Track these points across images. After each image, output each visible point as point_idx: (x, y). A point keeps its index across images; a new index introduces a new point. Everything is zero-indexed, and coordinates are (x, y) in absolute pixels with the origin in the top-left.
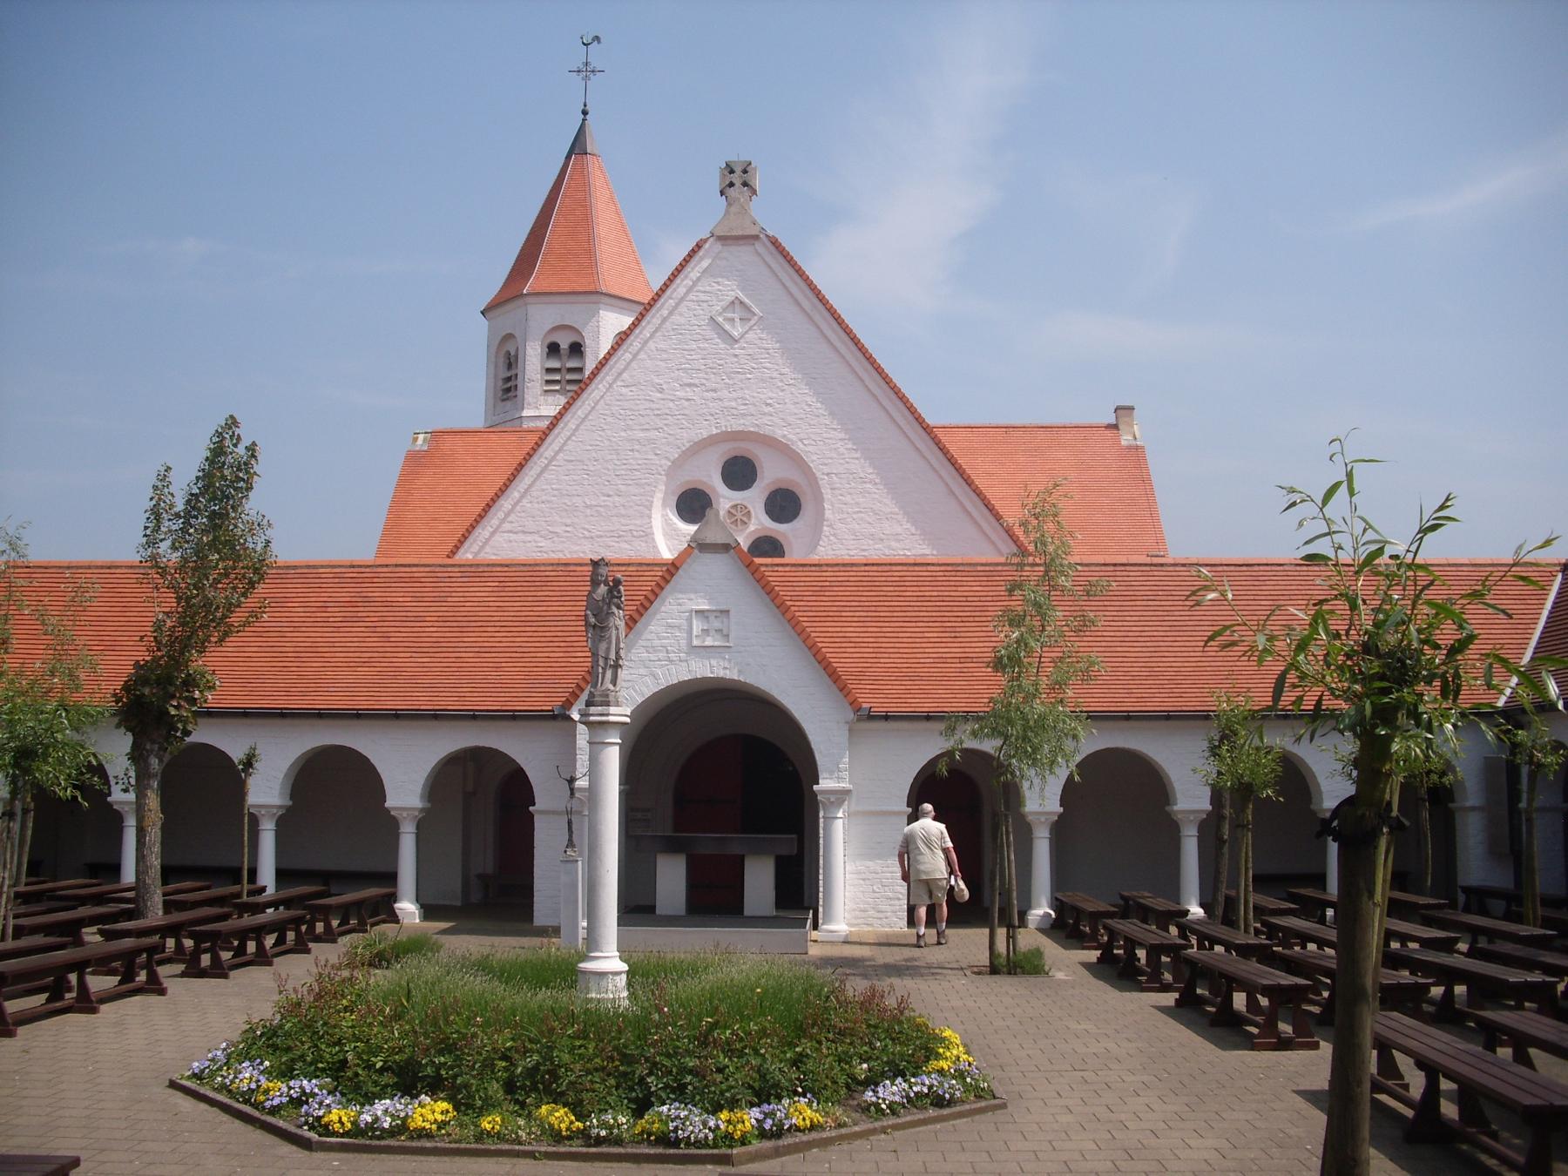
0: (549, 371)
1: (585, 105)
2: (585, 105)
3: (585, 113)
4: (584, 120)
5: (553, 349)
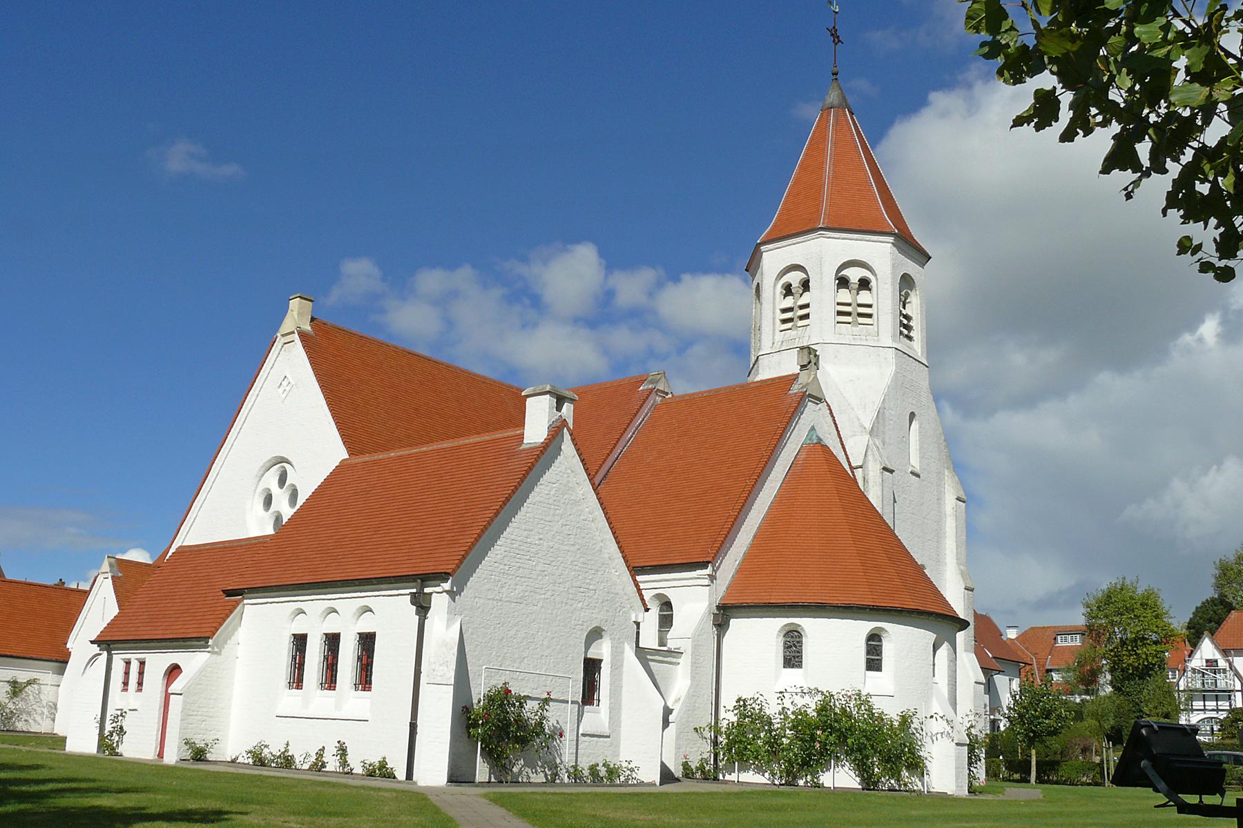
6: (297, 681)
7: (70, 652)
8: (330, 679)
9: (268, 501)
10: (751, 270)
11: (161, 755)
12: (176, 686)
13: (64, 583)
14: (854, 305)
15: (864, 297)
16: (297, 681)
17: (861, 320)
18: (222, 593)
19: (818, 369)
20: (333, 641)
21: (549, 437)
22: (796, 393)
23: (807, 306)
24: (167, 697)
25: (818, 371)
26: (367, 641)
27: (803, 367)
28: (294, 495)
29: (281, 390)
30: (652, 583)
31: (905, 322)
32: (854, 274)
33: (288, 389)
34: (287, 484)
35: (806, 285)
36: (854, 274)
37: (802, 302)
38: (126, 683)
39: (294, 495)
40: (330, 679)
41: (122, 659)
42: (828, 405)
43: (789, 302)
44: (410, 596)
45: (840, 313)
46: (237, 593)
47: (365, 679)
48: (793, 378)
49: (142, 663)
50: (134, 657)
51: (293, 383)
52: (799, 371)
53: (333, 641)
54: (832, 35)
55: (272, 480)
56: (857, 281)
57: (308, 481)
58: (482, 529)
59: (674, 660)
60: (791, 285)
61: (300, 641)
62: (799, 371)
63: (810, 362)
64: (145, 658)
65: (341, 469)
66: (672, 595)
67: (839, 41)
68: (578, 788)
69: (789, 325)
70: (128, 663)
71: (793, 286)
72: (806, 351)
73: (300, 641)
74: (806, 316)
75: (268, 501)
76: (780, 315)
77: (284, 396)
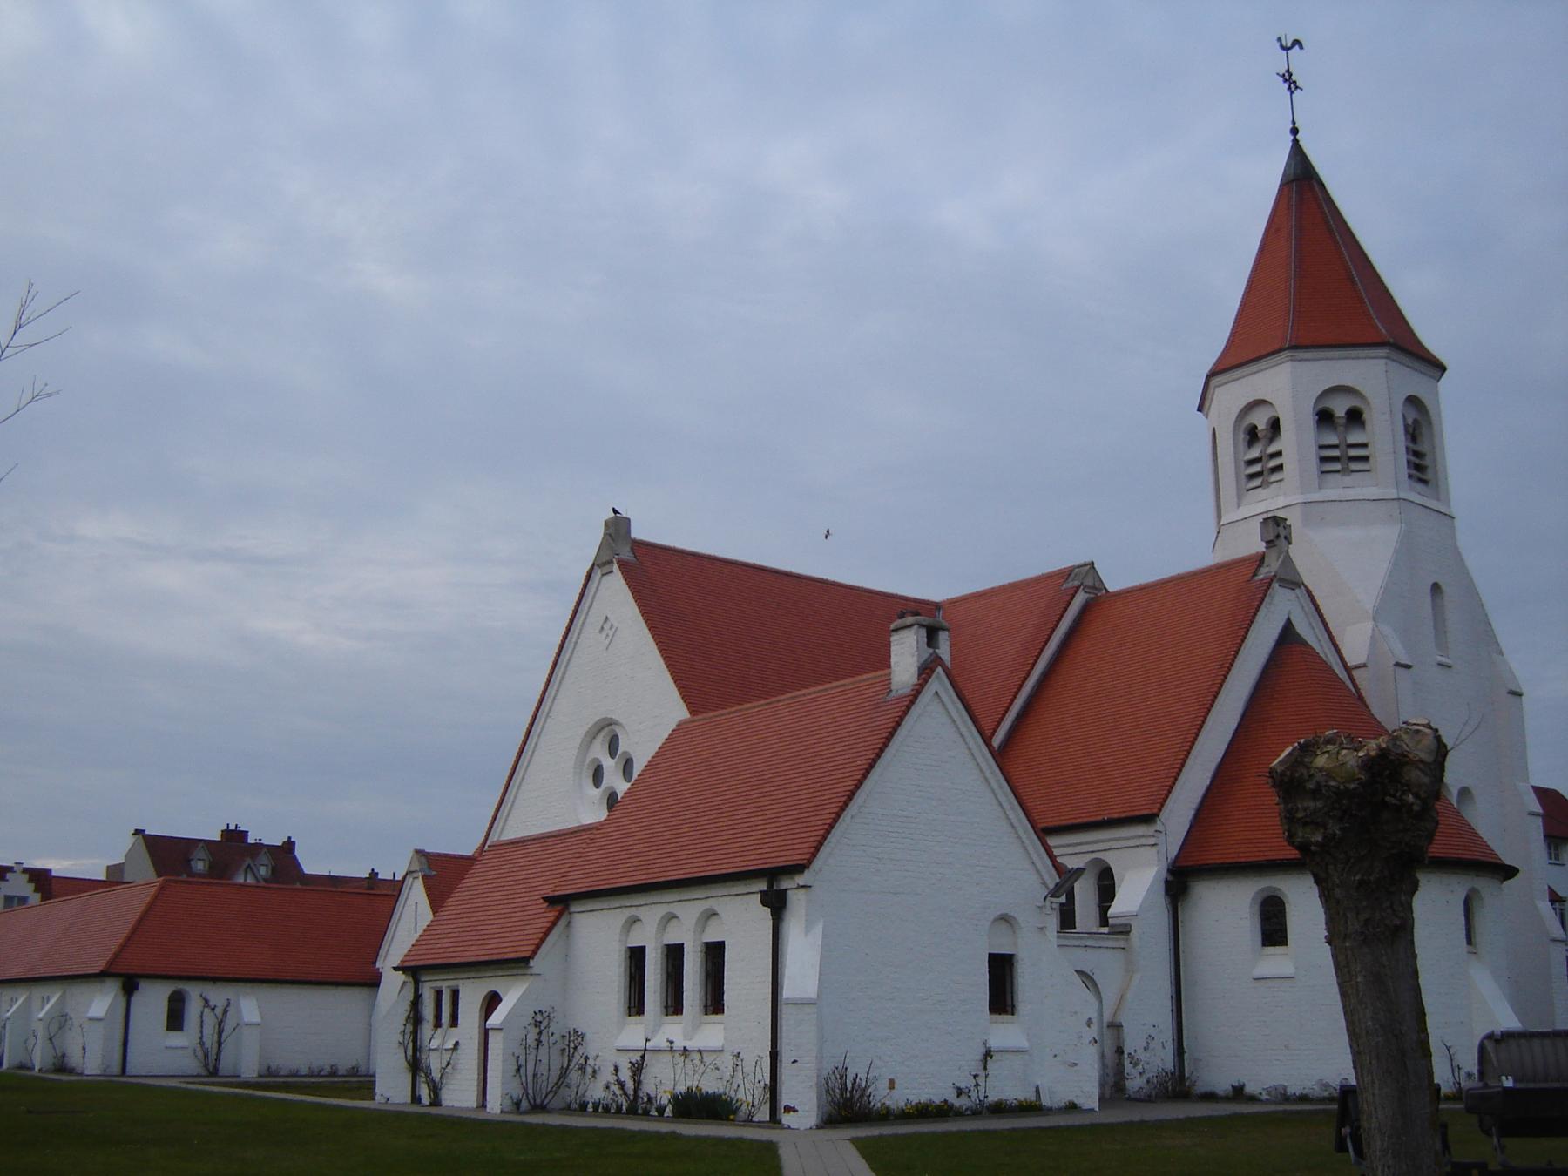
0: (1322, 447)
1: (1294, 123)
2: (1294, 123)
3: (1295, 131)
4: (1296, 142)
5: (1324, 418)
6: (636, 1006)
7: (381, 973)
8: (674, 1005)
9: (597, 776)
10: (1206, 410)
11: (483, 1105)
12: (496, 1018)
13: (377, 873)
14: (1343, 447)
15: (1355, 437)
16: (636, 1006)
17: (1354, 466)
18: (542, 901)
19: (1290, 543)
20: (674, 954)
21: (920, 682)
22: (1262, 580)
23: (1279, 454)
24: (485, 1033)
25: (1290, 546)
26: (715, 953)
27: (1270, 544)
28: (628, 765)
29: (604, 635)
30: (1075, 851)
31: (1417, 461)
32: (1340, 407)
33: (611, 633)
34: (619, 753)
35: (1275, 425)
36: (1340, 407)
37: (1272, 449)
38: (438, 1017)
39: (628, 765)
40: (674, 1005)
41: (431, 988)
42: (1309, 592)
43: (1255, 453)
44: (759, 895)
45: (1323, 460)
46: (561, 903)
47: (715, 1003)
48: (1261, 560)
49: (455, 994)
50: (446, 983)
51: (616, 625)
52: (1264, 550)
53: (674, 954)
54: (1295, 82)
55: (599, 751)
56: (1343, 415)
57: (643, 746)
58: (848, 796)
59: (1553, 857)
60: (1256, 427)
61: (637, 956)
62: (1264, 550)
63: (1278, 536)
64: (458, 986)
65: (680, 730)
66: (1112, 859)
67: (1297, 87)
68: (761, 1130)
69: (1257, 482)
70: (439, 993)
71: (1259, 428)
72: (1271, 523)
73: (637, 956)
74: (1280, 468)
75: (597, 776)
76: (1245, 470)
77: (607, 642)
